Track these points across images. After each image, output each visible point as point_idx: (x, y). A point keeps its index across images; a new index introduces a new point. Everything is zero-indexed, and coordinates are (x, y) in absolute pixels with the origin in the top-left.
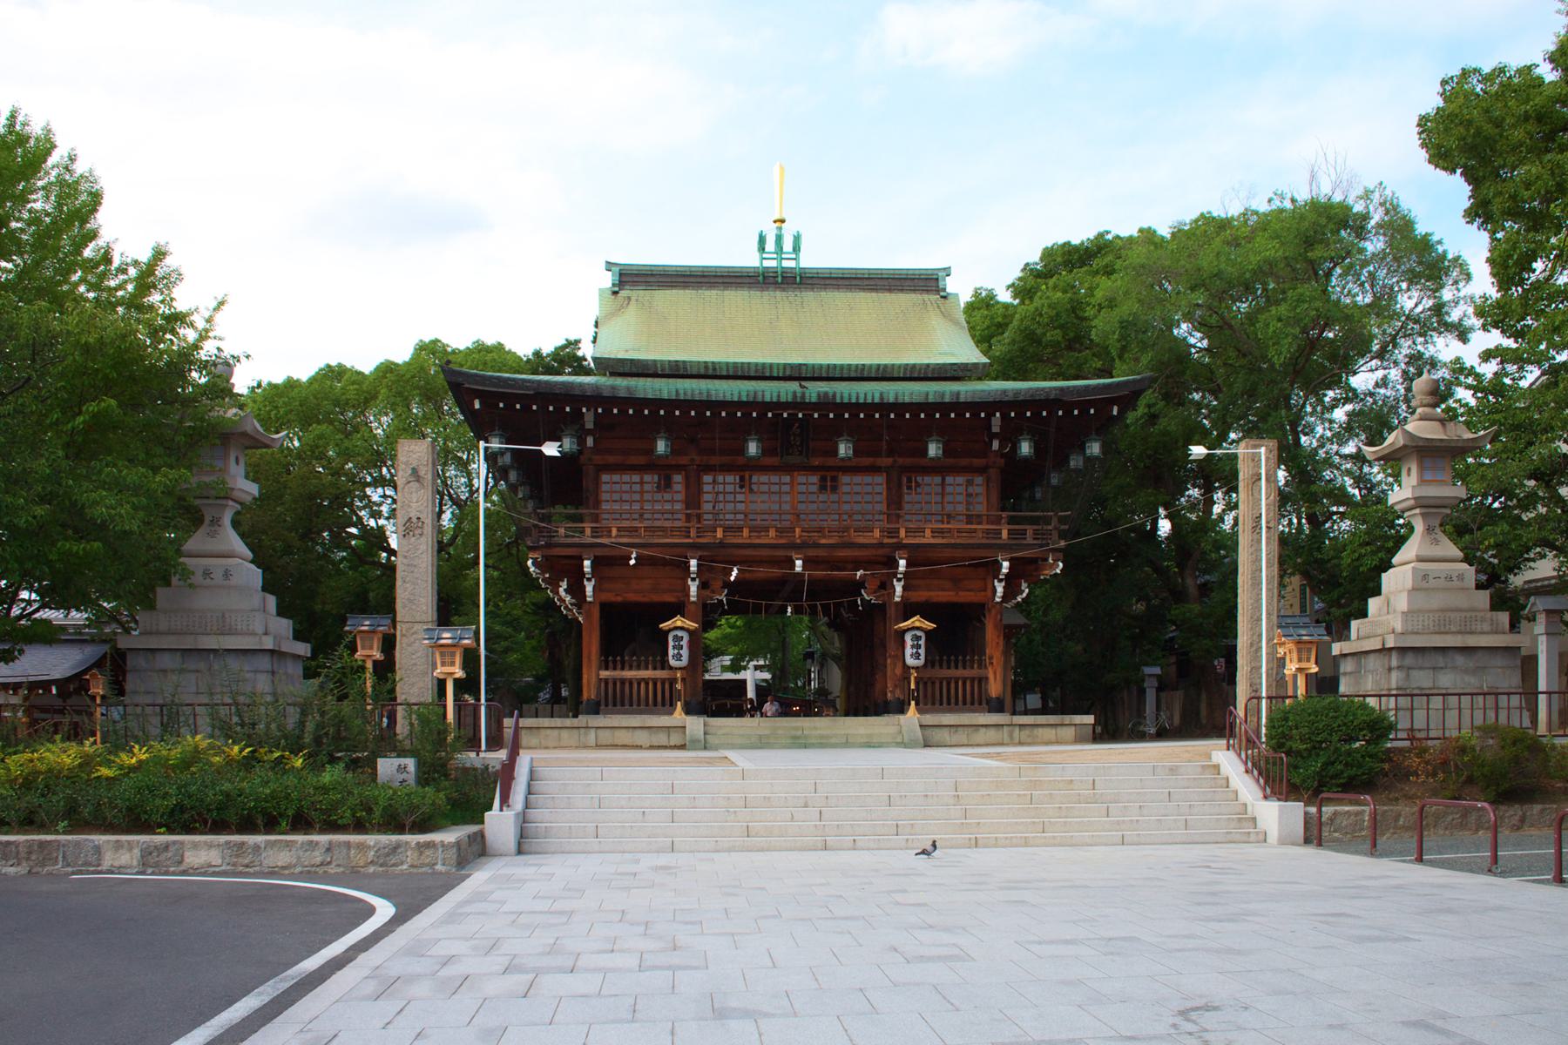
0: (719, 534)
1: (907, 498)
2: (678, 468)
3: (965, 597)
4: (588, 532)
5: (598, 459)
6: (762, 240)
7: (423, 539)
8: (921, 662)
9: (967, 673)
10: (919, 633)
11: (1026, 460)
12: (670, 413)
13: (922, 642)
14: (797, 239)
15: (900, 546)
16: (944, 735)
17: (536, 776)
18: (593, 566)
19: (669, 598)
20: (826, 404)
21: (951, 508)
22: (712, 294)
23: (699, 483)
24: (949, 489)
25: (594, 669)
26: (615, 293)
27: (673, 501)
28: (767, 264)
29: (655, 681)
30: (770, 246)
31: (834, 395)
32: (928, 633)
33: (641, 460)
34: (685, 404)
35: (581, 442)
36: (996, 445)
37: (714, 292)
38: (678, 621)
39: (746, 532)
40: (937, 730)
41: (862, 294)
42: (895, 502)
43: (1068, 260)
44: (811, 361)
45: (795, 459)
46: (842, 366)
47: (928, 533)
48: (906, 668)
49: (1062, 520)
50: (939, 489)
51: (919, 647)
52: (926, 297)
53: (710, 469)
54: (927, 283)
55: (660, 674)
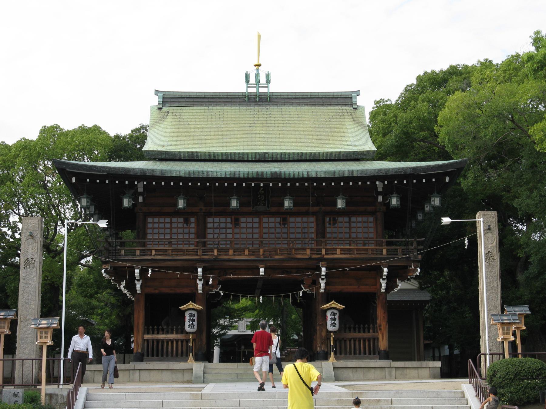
0: (215, 252)
1: (328, 230)
2: (193, 214)
3: (364, 289)
4: (138, 253)
6: (247, 76)
7: (34, 270)
8: (336, 328)
9: (366, 335)
10: (335, 311)
11: (395, 209)
12: (185, 184)
13: (337, 317)
14: (268, 75)
15: (322, 259)
16: (349, 373)
17: (89, 398)
18: (140, 273)
19: (186, 291)
20: (276, 178)
21: (355, 238)
22: (217, 109)
23: (205, 223)
24: (353, 225)
26: (160, 109)
27: (189, 233)
28: (251, 90)
29: (177, 341)
30: (252, 80)
33: (274, 209)
34: (195, 179)
35: (135, 199)
36: (380, 199)
37: (218, 107)
38: (191, 305)
39: (231, 252)
40: (345, 370)
41: (306, 107)
42: (321, 233)
43: (435, 84)
44: (271, 151)
45: (261, 208)
46: (289, 154)
47: (339, 251)
48: (329, 332)
49: (419, 243)
50: (347, 225)
52: (344, 108)
53: (210, 214)
54: (345, 100)
55: (180, 336)
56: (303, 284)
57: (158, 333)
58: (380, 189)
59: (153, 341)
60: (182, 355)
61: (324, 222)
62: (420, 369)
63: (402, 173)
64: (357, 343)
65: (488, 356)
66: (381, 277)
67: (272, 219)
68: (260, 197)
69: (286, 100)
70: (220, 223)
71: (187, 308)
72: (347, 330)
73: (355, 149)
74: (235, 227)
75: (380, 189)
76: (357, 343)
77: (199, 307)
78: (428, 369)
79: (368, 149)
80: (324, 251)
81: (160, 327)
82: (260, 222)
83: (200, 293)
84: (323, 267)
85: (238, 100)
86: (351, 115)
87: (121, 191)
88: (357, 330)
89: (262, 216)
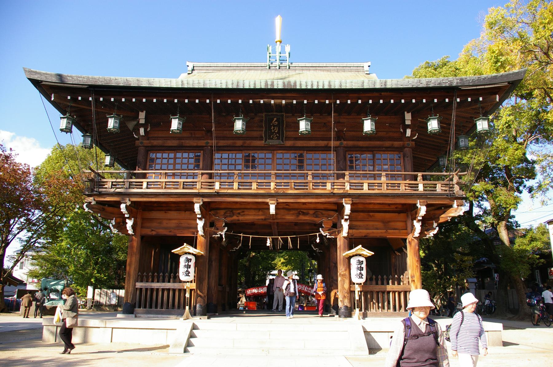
3: (392, 235)
5: (146, 142)
8: (362, 281)
10: (190, 257)
13: (364, 266)
25: (131, 281)
31: (295, 83)
32: (368, 259)
36: (409, 132)
38: (187, 248)
51: (361, 269)
53: (220, 149)
56: (322, 227)
57: (153, 281)
58: (408, 122)
59: (147, 289)
60: (179, 307)
63: (447, 85)
67: (287, 155)
68: (274, 129)
76: (386, 297)
84: (346, 203)
85: (261, 68)
89: (275, 152)
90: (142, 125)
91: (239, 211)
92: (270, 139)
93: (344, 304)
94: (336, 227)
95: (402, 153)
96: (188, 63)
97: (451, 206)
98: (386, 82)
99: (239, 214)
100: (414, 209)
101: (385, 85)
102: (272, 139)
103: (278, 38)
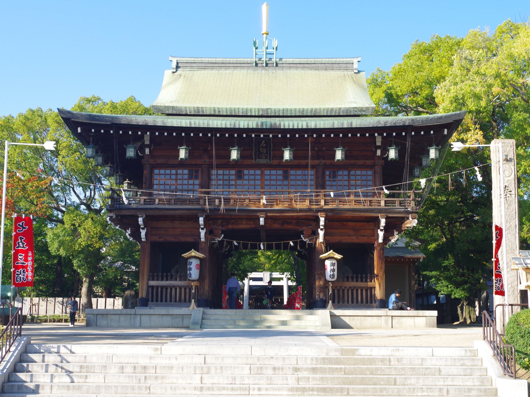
5: (151, 161)
18: (144, 221)
19: (190, 239)
22: (224, 72)
31: (280, 125)
33: (275, 162)
36: (379, 152)
37: (228, 71)
38: (193, 253)
41: (310, 72)
50: (346, 178)
52: (346, 73)
56: (303, 234)
58: (379, 143)
61: (324, 175)
62: (416, 318)
64: (355, 292)
65: (23, 327)
66: (379, 228)
69: (291, 65)
70: (223, 175)
71: (189, 256)
72: (346, 279)
73: (355, 105)
74: (238, 179)
75: (379, 143)
76: (355, 292)
77: (201, 255)
78: (425, 318)
79: (367, 106)
80: (322, 203)
81: (169, 274)
82: (262, 174)
83: (203, 242)
84: (321, 217)
85: (247, 65)
86: (352, 78)
87: (125, 141)
88: (355, 279)
90: (147, 146)
91: (233, 221)
92: (259, 158)
93: (320, 297)
94: (315, 234)
95: (373, 170)
96: (170, 58)
97: (408, 218)
98: (351, 123)
99: (233, 223)
100: (377, 221)
101: (351, 125)
102: (261, 158)
103: (264, 31)
